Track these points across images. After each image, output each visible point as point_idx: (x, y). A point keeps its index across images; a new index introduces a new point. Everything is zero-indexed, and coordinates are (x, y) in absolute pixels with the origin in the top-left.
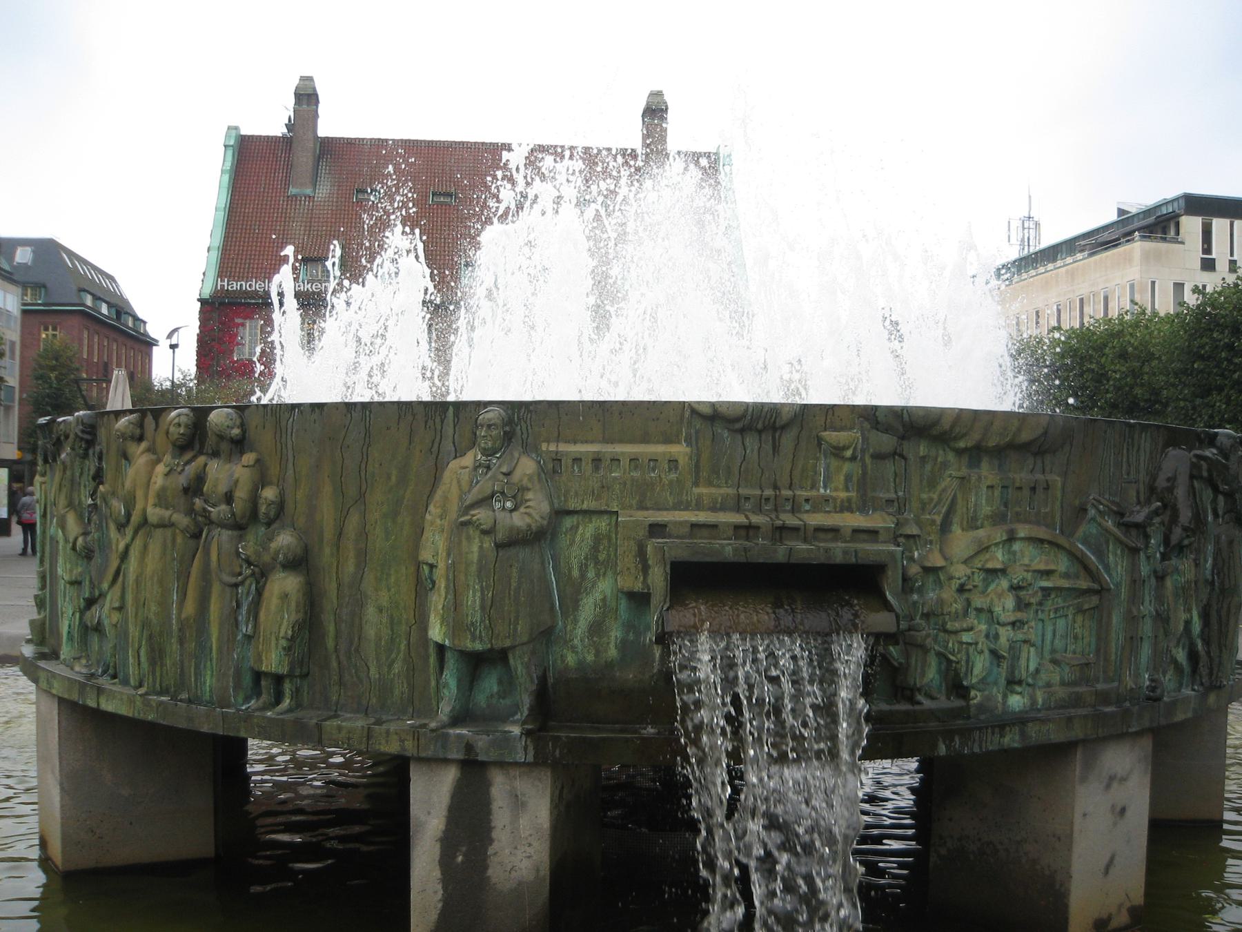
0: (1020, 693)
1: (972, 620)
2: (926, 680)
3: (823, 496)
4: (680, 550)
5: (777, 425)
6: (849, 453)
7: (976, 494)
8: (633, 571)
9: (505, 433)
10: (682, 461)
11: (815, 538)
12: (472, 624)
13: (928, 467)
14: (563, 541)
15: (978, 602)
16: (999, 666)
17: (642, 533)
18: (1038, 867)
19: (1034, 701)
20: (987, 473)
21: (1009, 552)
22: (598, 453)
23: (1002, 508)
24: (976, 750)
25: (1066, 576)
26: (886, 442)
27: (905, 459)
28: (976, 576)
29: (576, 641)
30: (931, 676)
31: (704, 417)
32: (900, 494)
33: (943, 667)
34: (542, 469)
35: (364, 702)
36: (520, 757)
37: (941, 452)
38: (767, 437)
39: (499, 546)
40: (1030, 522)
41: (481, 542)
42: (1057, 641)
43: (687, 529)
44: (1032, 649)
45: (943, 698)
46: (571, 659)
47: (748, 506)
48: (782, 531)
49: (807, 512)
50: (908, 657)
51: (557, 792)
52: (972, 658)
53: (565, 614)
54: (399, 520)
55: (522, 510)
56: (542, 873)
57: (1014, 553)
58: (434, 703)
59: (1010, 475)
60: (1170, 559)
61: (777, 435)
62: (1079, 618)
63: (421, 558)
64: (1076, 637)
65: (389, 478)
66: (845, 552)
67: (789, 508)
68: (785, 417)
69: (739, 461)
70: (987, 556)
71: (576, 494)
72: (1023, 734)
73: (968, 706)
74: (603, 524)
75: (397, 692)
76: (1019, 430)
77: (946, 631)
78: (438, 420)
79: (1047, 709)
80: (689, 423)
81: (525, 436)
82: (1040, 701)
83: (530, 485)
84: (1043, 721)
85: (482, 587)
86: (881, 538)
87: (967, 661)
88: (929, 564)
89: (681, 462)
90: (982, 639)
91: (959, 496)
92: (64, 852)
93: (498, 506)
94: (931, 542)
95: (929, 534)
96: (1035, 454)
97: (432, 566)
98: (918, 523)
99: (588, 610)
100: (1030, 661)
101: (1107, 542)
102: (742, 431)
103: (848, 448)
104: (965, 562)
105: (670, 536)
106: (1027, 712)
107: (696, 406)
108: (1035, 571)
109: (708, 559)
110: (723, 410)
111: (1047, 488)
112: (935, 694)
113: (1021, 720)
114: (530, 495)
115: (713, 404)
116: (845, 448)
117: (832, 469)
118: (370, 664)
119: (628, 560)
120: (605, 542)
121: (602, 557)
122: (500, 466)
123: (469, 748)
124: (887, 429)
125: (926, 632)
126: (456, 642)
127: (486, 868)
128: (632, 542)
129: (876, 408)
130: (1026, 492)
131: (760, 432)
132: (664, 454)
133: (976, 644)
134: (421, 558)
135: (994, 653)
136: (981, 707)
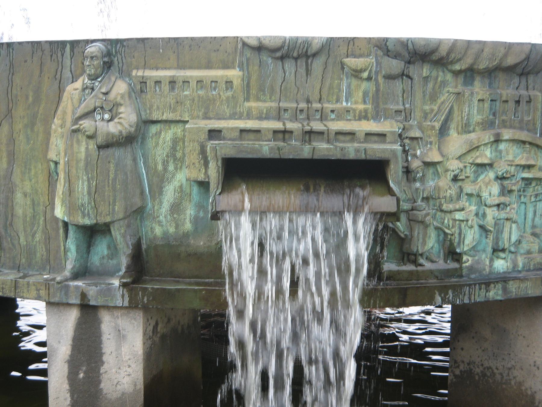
0: (505, 258)
1: (463, 202)
2: (426, 248)
3: (345, 108)
4: (228, 148)
5: (309, 53)
6: (365, 75)
7: (469, 106)
8: (197, 165)
9: (104, 63)
10: (236, 82)
11: (337, 140)
12: (82, 205)
13: (430, 85)
14: (150, 143)
15: (469, 188)
16: (487, 238)
17: (203, 136)
18: (523, 388)
19: (515, 265)
20: (479, 89)
21: (496, 150)
22: (174, 76)
23: (491, 117)
24: (466, 301)
26: (395, 65)
27: (411, 79)
28: (468, 169)
29: (161, 218)
30: (431, 245)
31: (272, 51)
32: (407, 106)
33: (441, 238)
34: (131, 89)
35: (18, 262)
36: (119, 303)
37: (441, 74)
38: (302, 63)
39: (100, 147)
40: (514, 128)
41: (87, 144)
42: (537, 219)
43: (237, 134)
44: (514, 226)
45: (441, 262)
46: (158, 231)
47: (286, 115)
48: (310, 135)
49: (333, 120)
50: (411, 230)
51: (151, 328)
52: (463, 231)
53: (153, 198)
54: (36, 129)
55: (116, 120)
56: (138, 387)
57: (501, 152)
58: (64, 262)
59: (499, 91)
61: (310, 61)
63: (49, 157)
65: (27, 98)
66: (357, 151)
67: (318, 117)
68: (315, 47)
69: (281, 81)
70: (478, 154)
71: (158, 108)
72: (505, 290)
73: (461, 268)
74: (178, 130)
75: (38, 255)
76: (506, 55)
77: (442, 211)
78: (59, 55)
79: (527, 271)
80: (242, 53)
81: (121, 65)
82: (521, 265)
83: (122, 102)
84: (522, 280)
85: (88, 178)
86: (388, 139)
87: (460, 234)
88: (428, 160)
89: (235, 83)
90: (471, 217)
91: (456, 108)
93: (98, 117)
94: (431, 143)
95: (430, 137)
96: (521, 75)
97: (56, 163)
99: (169, 194)
100: (511, 234)
102: (282, 58)
103: (365, 70)
104: (459, 158)
105: (224, 139)
106: (509, 273)
107: (246, 40)
108: (517, 165)
109: (250, 156)
110: (266, 42)
111: (529, 102)
112: (434, 259)
113: (504, 279)
114: (122, 109)
115: (259, 39)
116: (362, 71)
117: (353, 87)
118: (20, 234)
119: (193, 157)
120: (181, 144)
121: (179, 155)
122: (100, 88)
123: (83, 296)
124: (397, 56)
125: (425, 211)
126: (71, 219)
127: (100, 382)
128: (196, 144)
129: (386, 40)
130: (512, 105)
131: (296, 59)
132: (222, 77)
133: (467, 221)
134: (49, 157)
136: (471, 269)
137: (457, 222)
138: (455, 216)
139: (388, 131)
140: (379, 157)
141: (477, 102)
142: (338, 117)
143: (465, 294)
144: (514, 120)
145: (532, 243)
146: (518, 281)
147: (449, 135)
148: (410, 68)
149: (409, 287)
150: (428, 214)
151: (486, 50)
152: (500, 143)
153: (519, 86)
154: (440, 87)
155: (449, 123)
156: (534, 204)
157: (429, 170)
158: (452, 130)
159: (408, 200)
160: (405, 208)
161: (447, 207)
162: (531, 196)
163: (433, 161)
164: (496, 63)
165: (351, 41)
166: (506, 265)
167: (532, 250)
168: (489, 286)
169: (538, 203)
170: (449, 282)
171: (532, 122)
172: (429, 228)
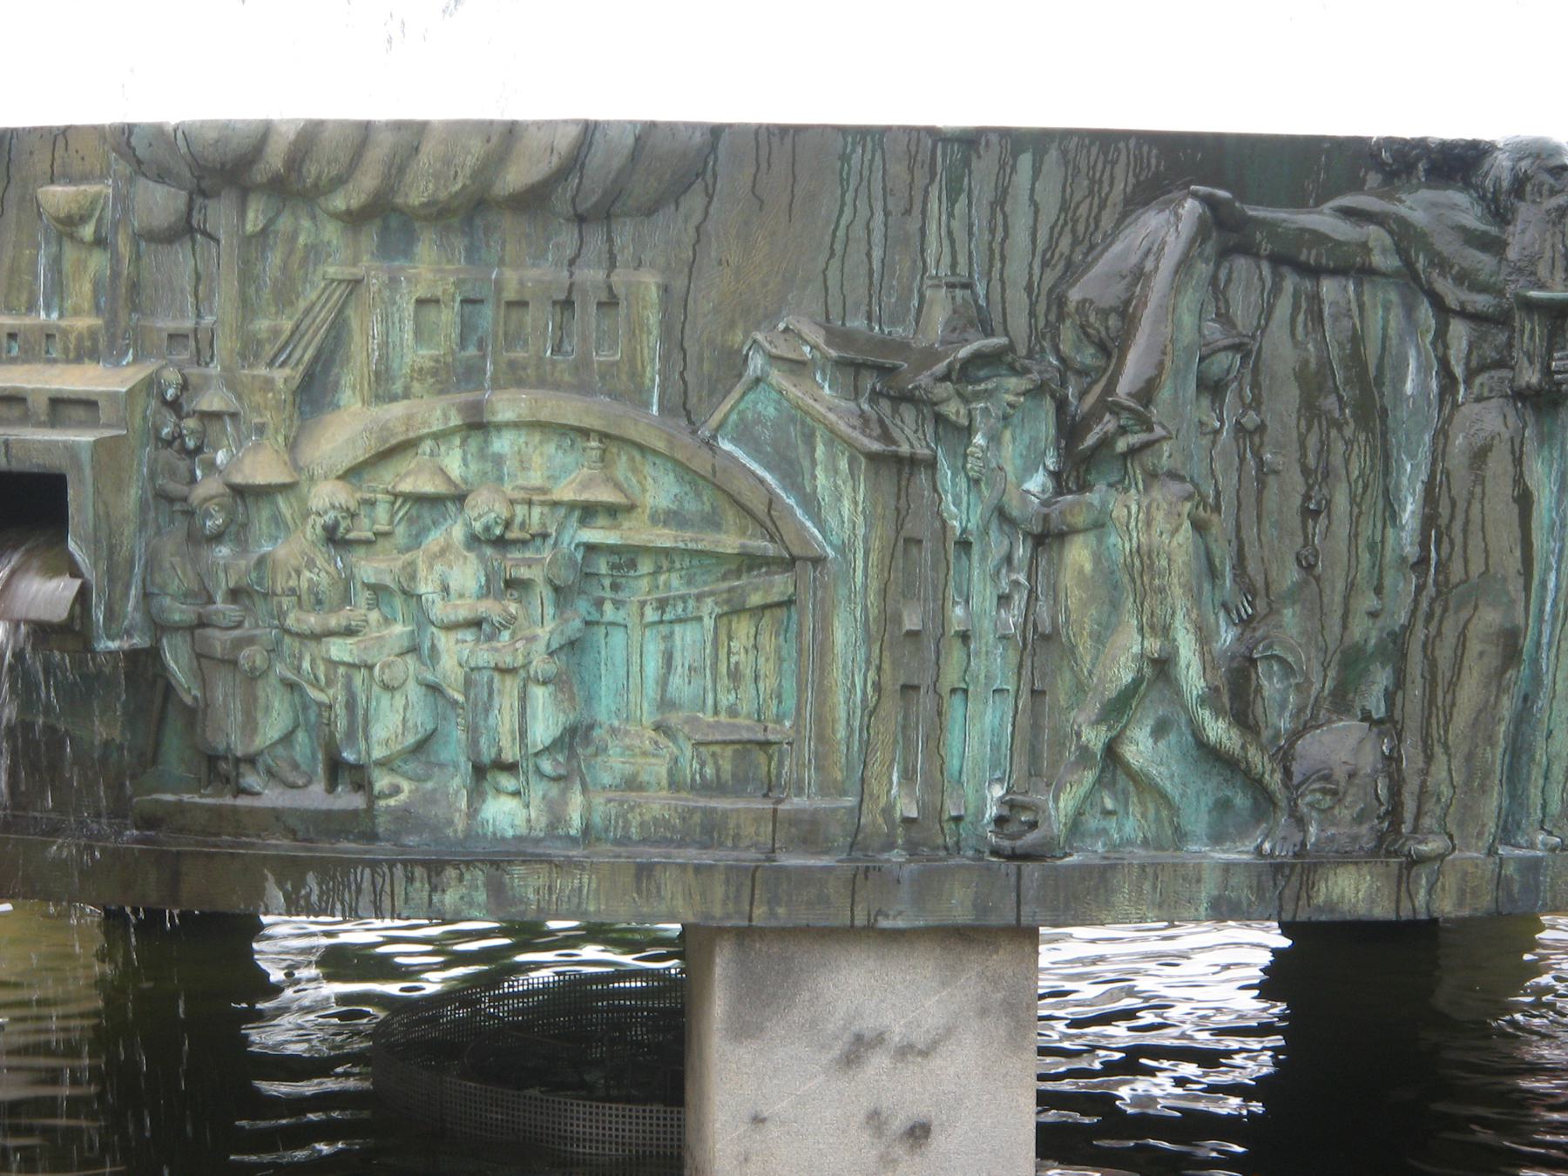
0: (516, 794)
1: (360, 610)
3: (42, 327)
6: (88, 232)
7: (385, 319)
13: (275, 258)
19: (556, 819)
20: (430, 267)
21: (482, 455)
25: (672, 518)
37: (306, 223)
40: (557, 386)
42: (676, 681)
45: (318, 788)
50: (204, 684)
57: (498, 460)
60: (1084, 487)
62: (743, 628)
64: (735, 675)
73: (370, 808)
87: (351, 705)
88: (238, 479)
92: (258, 1090)
94: (261, 429)
98: (231, 383)
101: (809, 438)
103: (83, 219)
106: (537, 841)
111: (610, 303)
117: (67, 266)
124: (163, 176)
129: (128, 130)
135: (434, 689)
136: (403, 817)
137: (341, 670)
138: (328, 651)
139: (101, 393)
140: (38, 465)
141: (411, 308)
142: (26, 352)
143: (359, 890)
144: (554, 363)
145: (645, 754)
146: (545, 866)
147: (338, 407)
148: (209, 211)
149: (186, 853)
150: (251, 641)
151: (429, 150)
152: (494, 433)
153: (578, 255)
154: (304, 262)
155: (336, 370)
156: (664, 629)
157: (259, 510)
158: (349, 392)
159: (185, 595)
160: (177, 617)
161: (298, 620)
162: (643, 604)
163: (250, 481)
164: (458, 186)
165: (60, 137)
166: (521, 815)
167: (644, 777)
168: (438, 874)
169: (678, 629)
170: (334, 850)
171: (626, 368)
172: (260, 683)
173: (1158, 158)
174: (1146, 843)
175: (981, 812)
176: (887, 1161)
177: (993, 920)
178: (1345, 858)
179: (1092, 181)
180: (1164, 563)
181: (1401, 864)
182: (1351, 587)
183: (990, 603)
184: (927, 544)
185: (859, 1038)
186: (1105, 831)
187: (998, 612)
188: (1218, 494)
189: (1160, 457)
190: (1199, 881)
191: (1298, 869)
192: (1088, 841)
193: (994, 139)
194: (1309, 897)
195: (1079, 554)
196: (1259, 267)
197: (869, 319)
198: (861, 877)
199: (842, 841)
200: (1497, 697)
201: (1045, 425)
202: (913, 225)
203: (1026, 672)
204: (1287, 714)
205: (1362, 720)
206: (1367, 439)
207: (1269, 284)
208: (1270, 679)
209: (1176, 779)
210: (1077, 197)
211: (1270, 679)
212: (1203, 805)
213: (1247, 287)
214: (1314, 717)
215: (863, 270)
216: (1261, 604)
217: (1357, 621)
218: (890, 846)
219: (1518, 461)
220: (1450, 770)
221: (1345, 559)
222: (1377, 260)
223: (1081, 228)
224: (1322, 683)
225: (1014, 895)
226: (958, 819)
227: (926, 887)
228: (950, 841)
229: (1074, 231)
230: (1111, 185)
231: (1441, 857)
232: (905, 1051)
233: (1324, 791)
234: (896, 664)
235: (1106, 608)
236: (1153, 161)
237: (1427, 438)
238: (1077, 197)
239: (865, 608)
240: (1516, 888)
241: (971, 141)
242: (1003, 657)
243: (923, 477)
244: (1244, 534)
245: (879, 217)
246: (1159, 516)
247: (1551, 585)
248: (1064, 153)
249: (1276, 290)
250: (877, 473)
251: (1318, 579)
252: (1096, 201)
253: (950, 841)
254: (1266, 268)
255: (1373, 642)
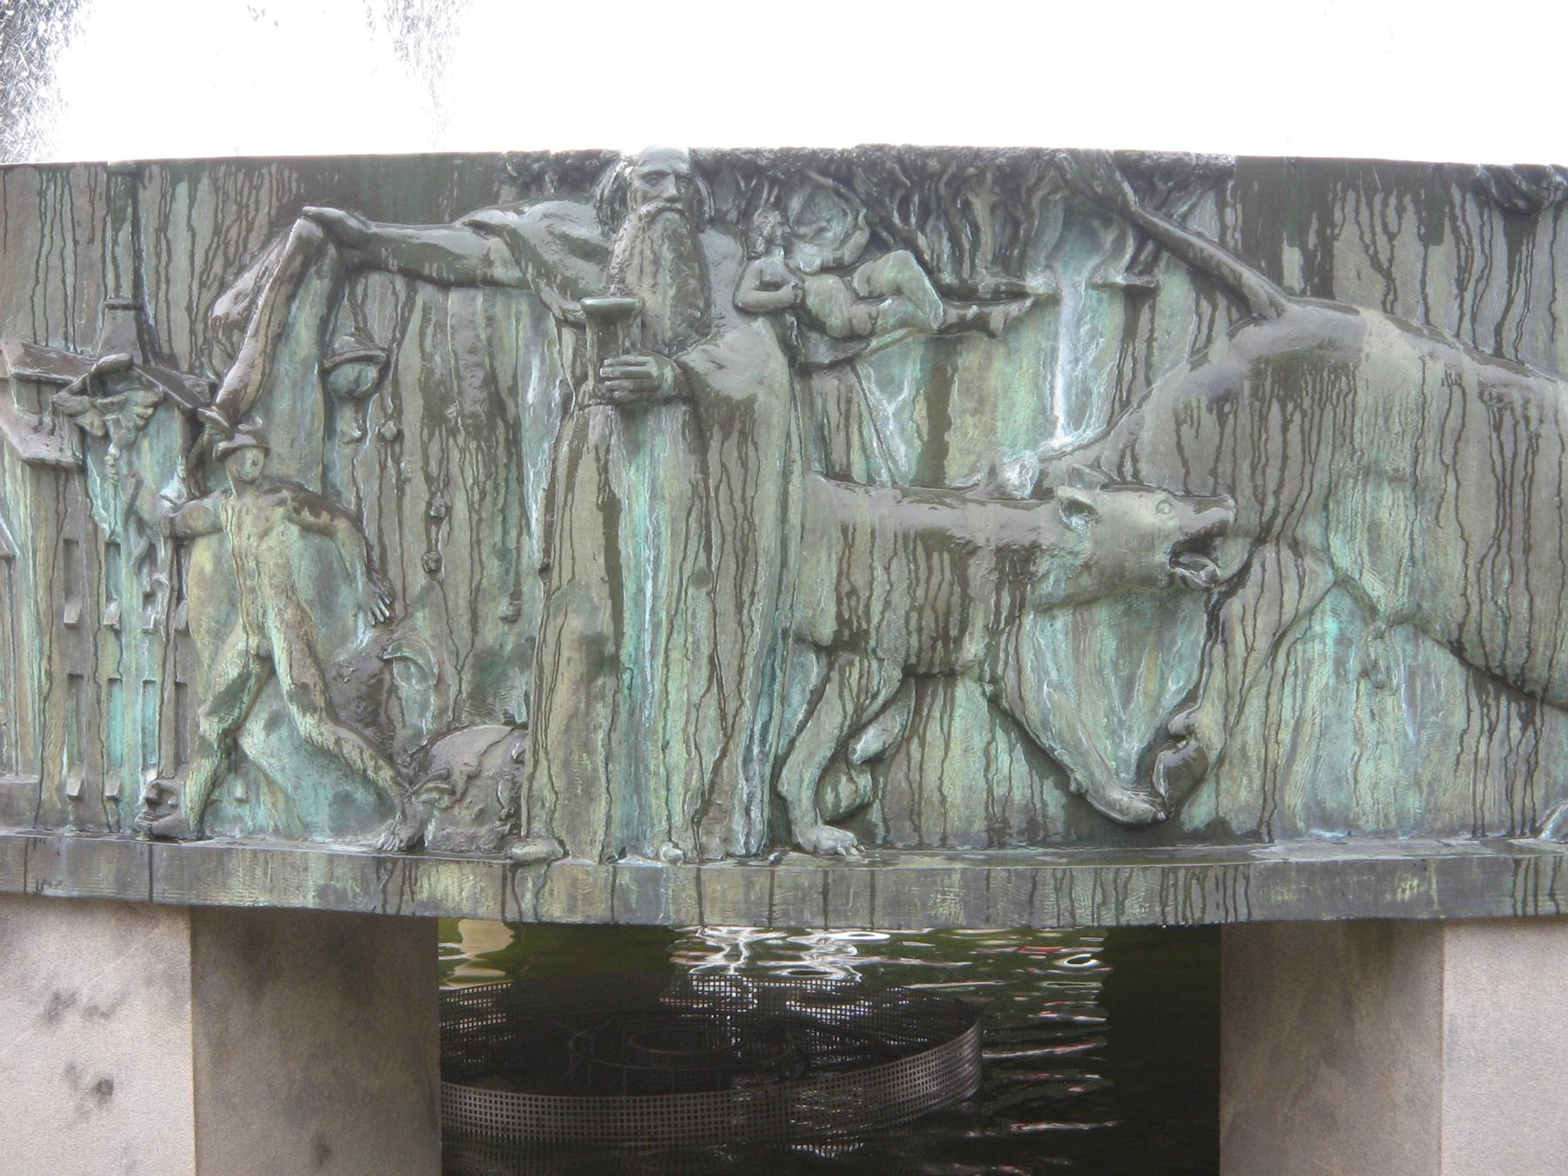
60: (205, 493)
173: (297, 181)
174: (276, 831)
175: (136, 793)
176: (83, 1114)
177: (131, 895)
178: (458, 857)
179: (240, 205)
180: (253, 564)
181: (504, 866)
182: (476, 595)
183: (138, 601)
184: (83, 545)
185: (57, 997)
186: (240, 819)
187: (144, 608)
188: (359, 499)
189: (243, 465)
190: (306, 869)
191: (400, 864)
192: (227, 826)
193: (156, 170)
194: (413, 893)
195: (201, 557)
196: (392, 283)
197: (66, 339)
198: (31, 847)
199: (30, 815)
200: (588, 704)
201: (174, 431)
202: (96, 253)
203: (170, 666)
204: (429, 715)
205: (506, 724)
206: (479, 448)
207: (402, 298)
208: (408, 680)
209: (288, 771)
210: (227, 223)
211: (408, 680)
212: (322, 797)
213: (382, 302)
214: (457, 718)
215: (60, 297)
216: (398, 606)
217: (489, 626)
218: (62, 822)
219: (604, 469)
220: (550, 776)
221: (468, 564)
222: (499, 272)
223: (232, 250)
224: (459, 686)
225: (147, 872)
226: (115, 800)
227: (81, 857)
228: (112, 820)
229: (226, 254)
230: (257, 210)
231: (546, 861)
232: (92, 1012)
233: (442, 791)
234: (62, 655)
235: (225, 607)
236: (294, 184)
237: (546, 446)
238: (227, 223)
239: (36, 602)
240: (633, 898)
241: (135, 174)
242: (150, 651)
243: (76, 484)
244: (386, 540)
245: (70, 245)
246: (248, 520)
247: (649, 593)
248: (215, 180)
249: (410, 304)
250: (38, 481)
251: (441, 584)
252: (244, 224)
253: (112, 820)
254: (400, 284)
255: (509, 648)
